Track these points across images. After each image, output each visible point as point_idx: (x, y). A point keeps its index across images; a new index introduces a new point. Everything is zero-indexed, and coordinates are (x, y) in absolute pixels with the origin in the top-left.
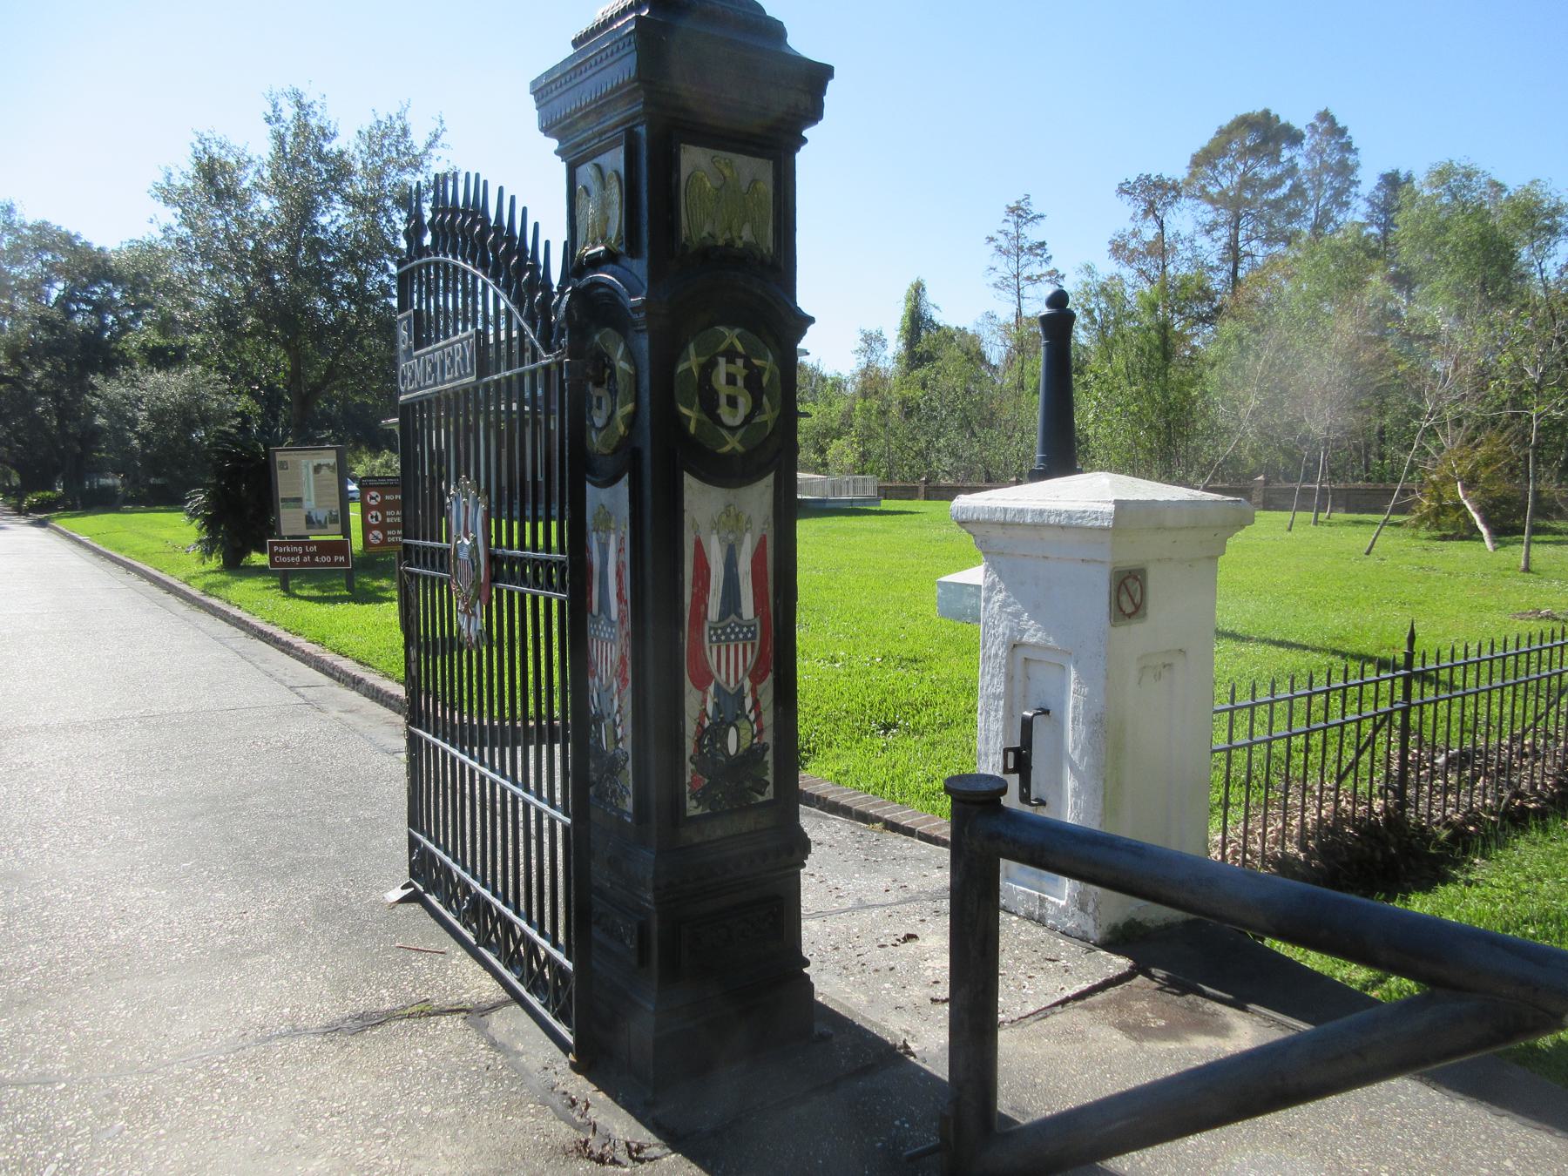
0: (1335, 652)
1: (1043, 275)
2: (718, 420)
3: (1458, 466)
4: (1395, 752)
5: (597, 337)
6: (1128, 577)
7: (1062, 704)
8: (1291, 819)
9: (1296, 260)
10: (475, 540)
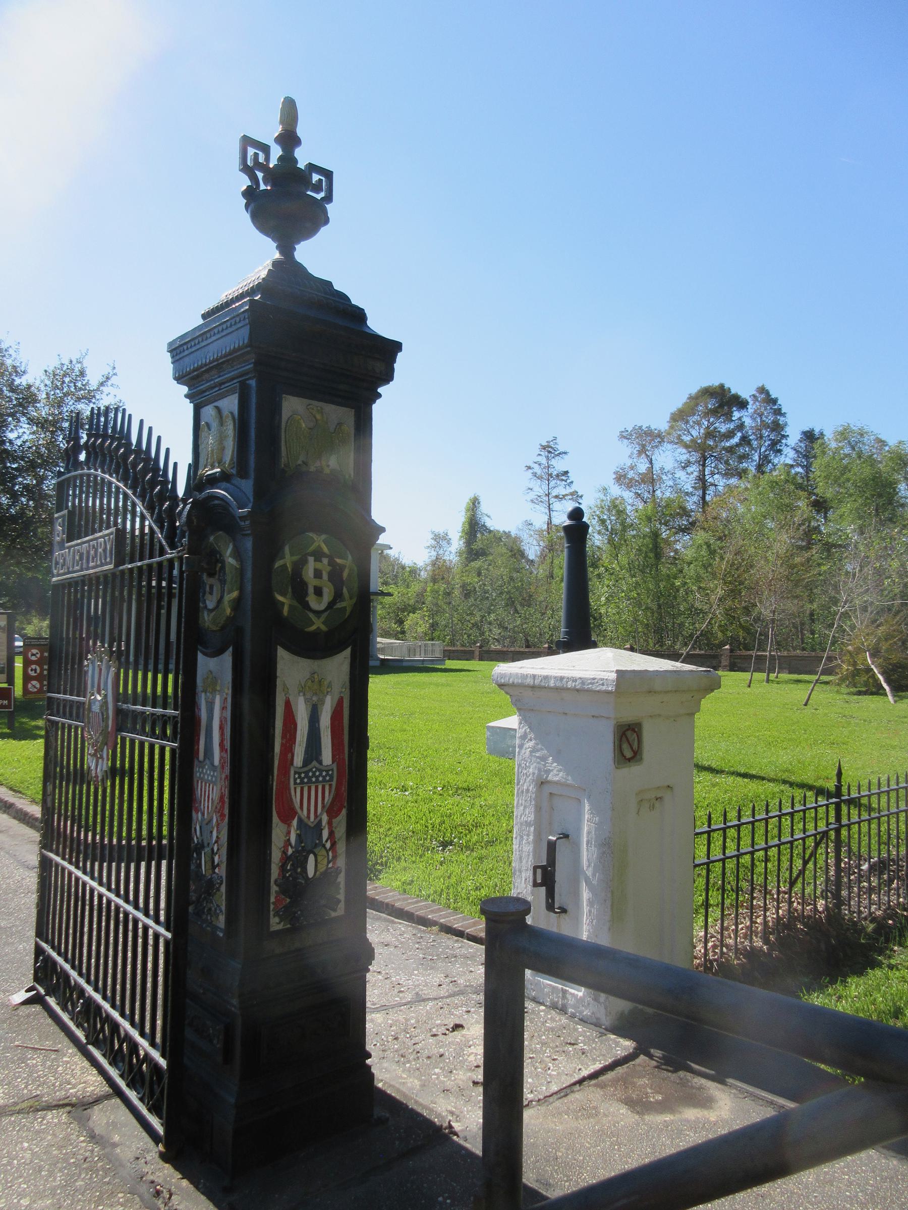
0: (785, 782)
1: (567, 495)
2: (306, 606)
3: (867, 640)
4: (831, 861)
5: (212, 538)
6: (628, 730)
7: (579, 829)
8: (757, 917)
9: (746, 489)
10: (106, 696)
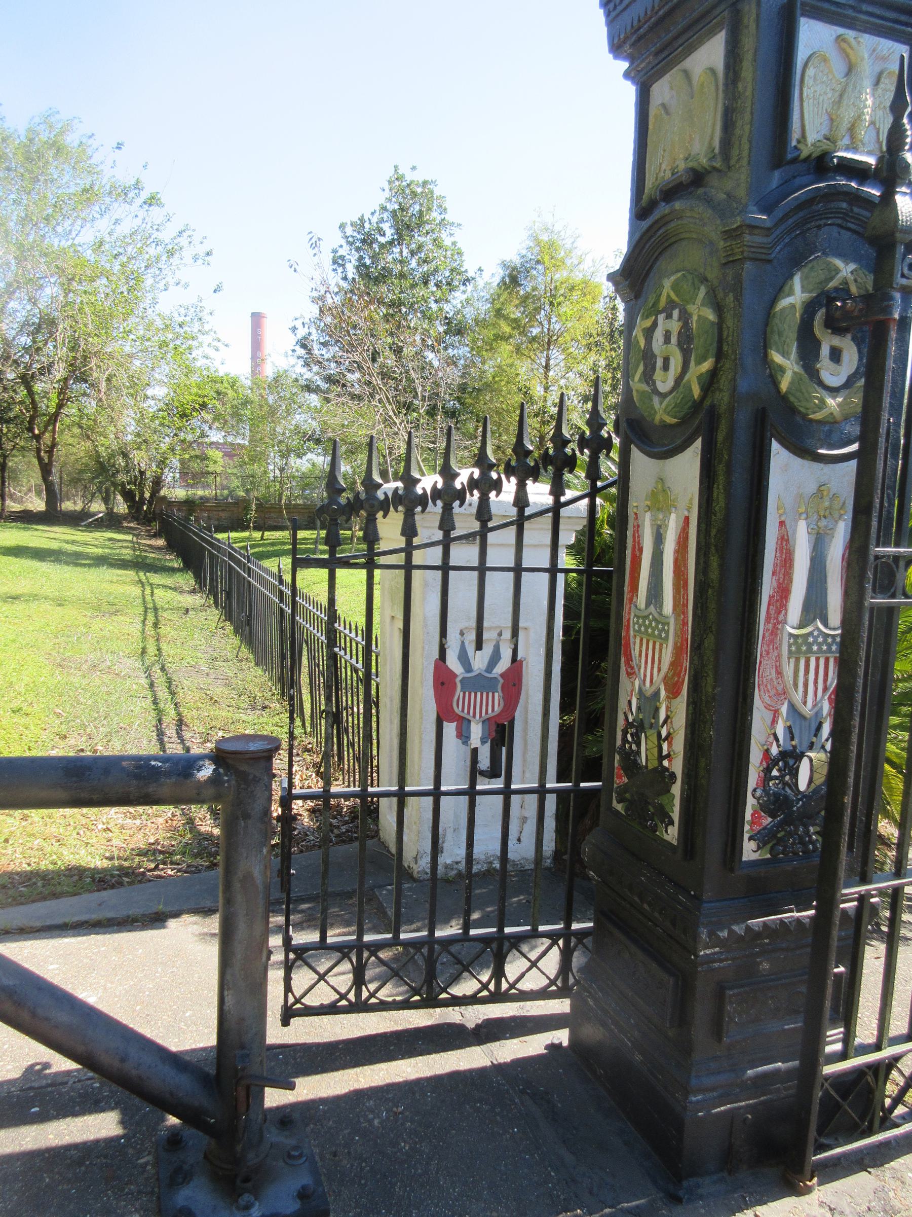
2: (813, 374)
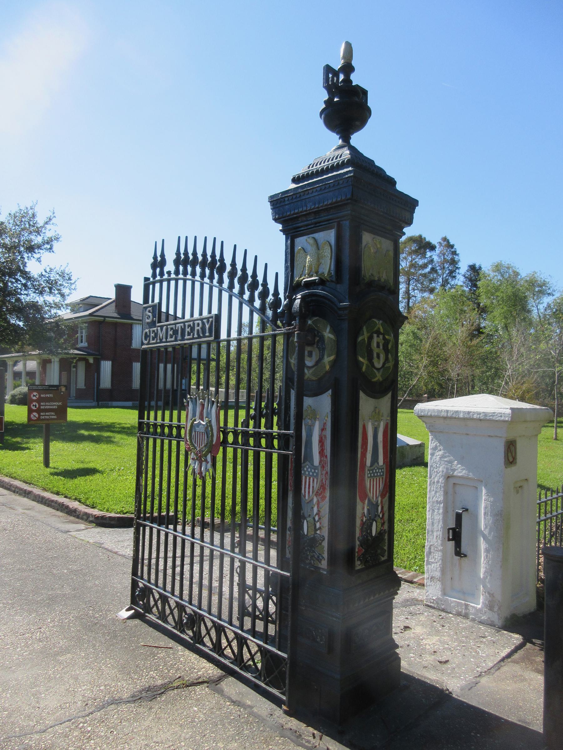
2: (373, 366)
